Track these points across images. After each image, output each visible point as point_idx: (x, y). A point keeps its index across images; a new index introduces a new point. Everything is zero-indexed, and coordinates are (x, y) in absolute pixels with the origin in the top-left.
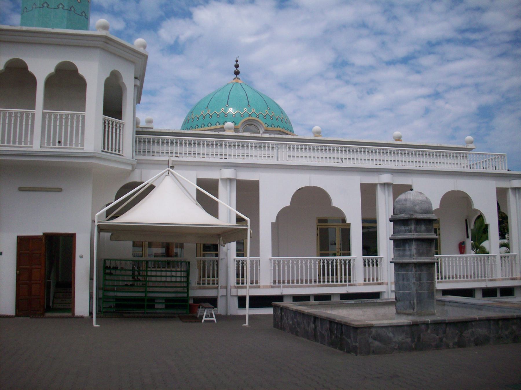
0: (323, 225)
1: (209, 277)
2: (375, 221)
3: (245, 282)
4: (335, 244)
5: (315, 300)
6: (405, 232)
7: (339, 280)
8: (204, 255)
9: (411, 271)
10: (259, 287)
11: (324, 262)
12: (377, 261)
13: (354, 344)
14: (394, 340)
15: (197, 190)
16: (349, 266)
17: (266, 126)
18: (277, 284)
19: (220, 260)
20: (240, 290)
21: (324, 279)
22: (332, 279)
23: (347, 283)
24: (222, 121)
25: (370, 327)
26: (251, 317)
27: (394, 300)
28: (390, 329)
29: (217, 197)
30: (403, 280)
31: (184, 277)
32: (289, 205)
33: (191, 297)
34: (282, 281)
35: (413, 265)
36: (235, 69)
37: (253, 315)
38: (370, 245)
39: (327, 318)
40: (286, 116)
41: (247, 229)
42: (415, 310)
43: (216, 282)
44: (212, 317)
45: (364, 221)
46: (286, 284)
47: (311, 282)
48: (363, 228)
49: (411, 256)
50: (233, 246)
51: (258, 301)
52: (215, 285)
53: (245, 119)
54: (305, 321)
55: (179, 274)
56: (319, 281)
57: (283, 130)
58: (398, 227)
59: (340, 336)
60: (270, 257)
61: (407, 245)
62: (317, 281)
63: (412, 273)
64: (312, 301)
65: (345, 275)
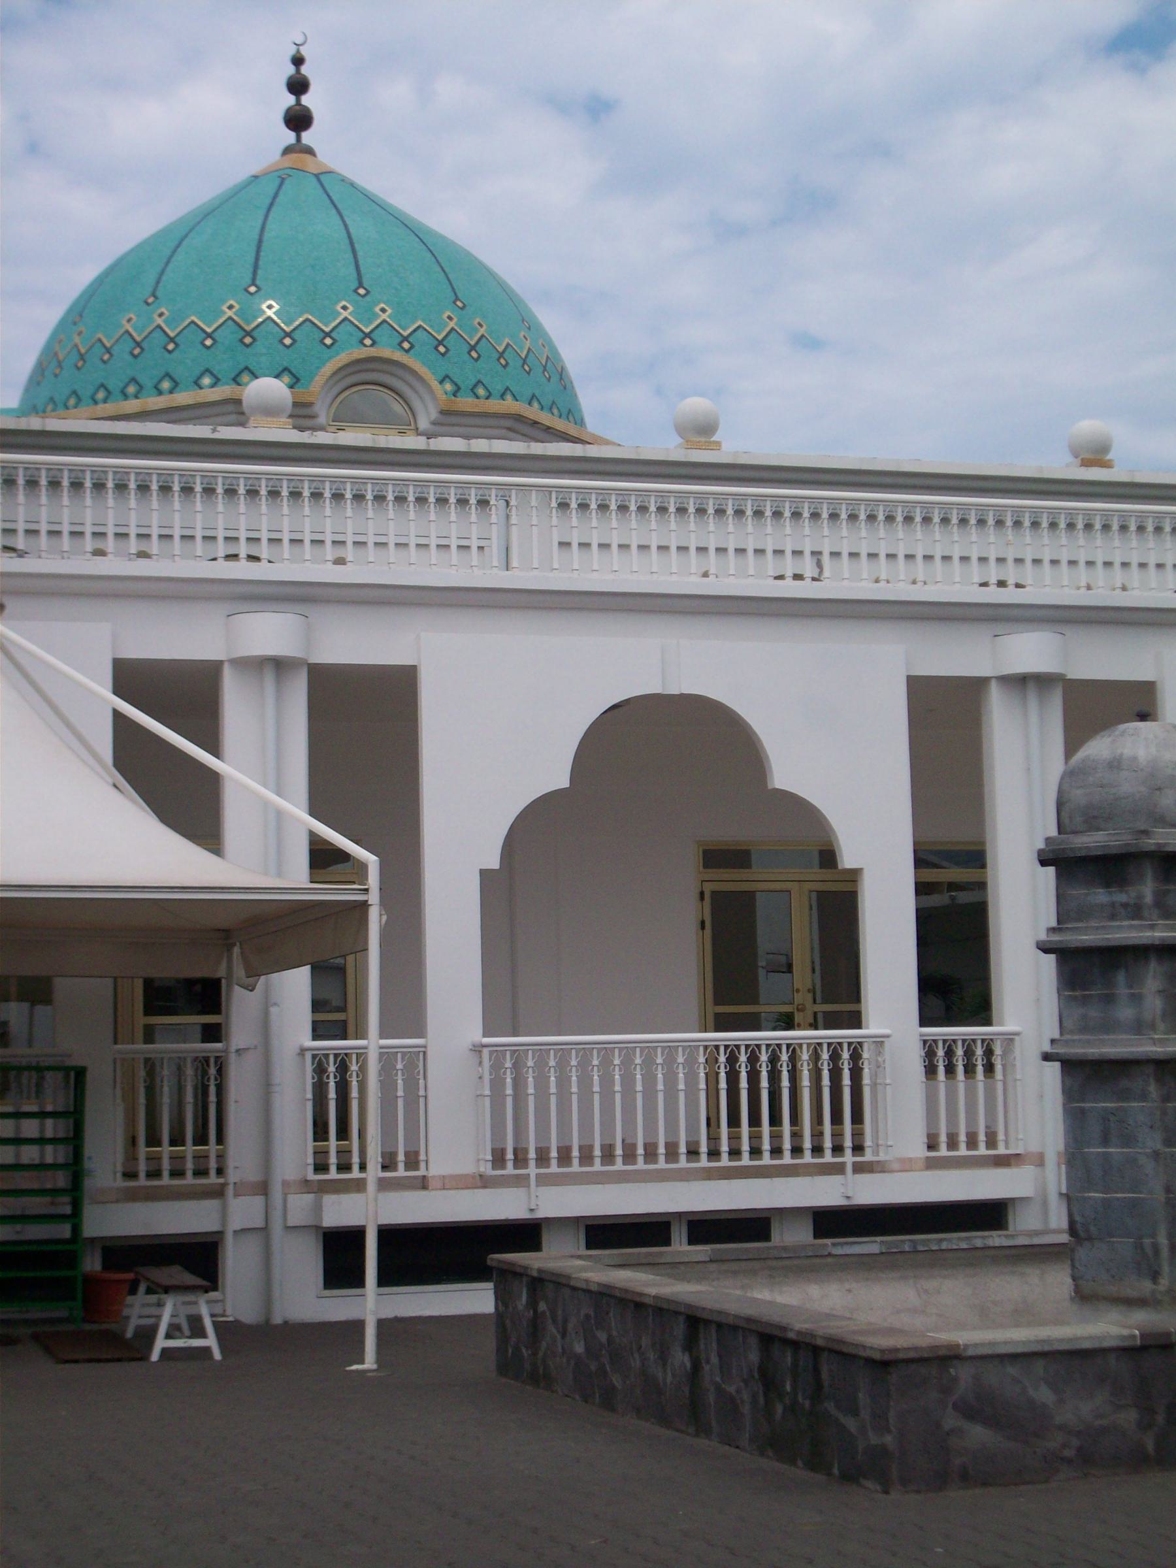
0: (730, 880)
1: (177, 1140)
2: (976, 857)
3: (356, 1159)
4: (789, 968)
5: (690, 1243)
6: (1113, 917)
7: (807, 1144)
8: (149, 1035)
9: (1144, 1097)
10: (423, 1184)
11: (732, 1059)
12: (989, 1052)
13: (874, 1440)
14: (1058, 1420)
15: (117, 715)
16: (856, 1074)
17: (442, 381)
18: (510, 1169)
19: (233, 1057)
20: (329, 1199)
21: (734, 1138)
22: (776, 1137)
23: (848, 1158)
24: (225, 368)
25: (946, 1359)
26: (389, 1329)
27: (1064, 1238)
28: (1039, 1366)
29: (216, 751)
30: (1105, 1142)
31: (53, 1141)
32: (564, 782)
33: (93, 1240)
34: (532, 1154)
35: (1150, 1069)
36: (291, 100)
37: (398, 1320)
38: (954, 979)
39: (749, 1320)
40: (548, 343)
41: (364, 905)
42: (1164, 1283)
43: (213, 1165)
44: (200, 1332)
45: (924, 858)
46: (554, 1168)
47: (672, 1155)
48: (921, 889)
49: (1139, 1027)
50: (294, 987)
51: (422, 1253)
52: (210, 1181)
53: (343, 358)
54: (645, 1341)
55: (30, 1128)
56: (709, 1155)
57: (532, 412)
58: (1077, 892)
59: (811, 1407)
60: (475, 1034)
61: (1121, 977)
62: (704, 1149)
63: (1143, 1107)
64: (680, 1246)
65: (837, 1118)
